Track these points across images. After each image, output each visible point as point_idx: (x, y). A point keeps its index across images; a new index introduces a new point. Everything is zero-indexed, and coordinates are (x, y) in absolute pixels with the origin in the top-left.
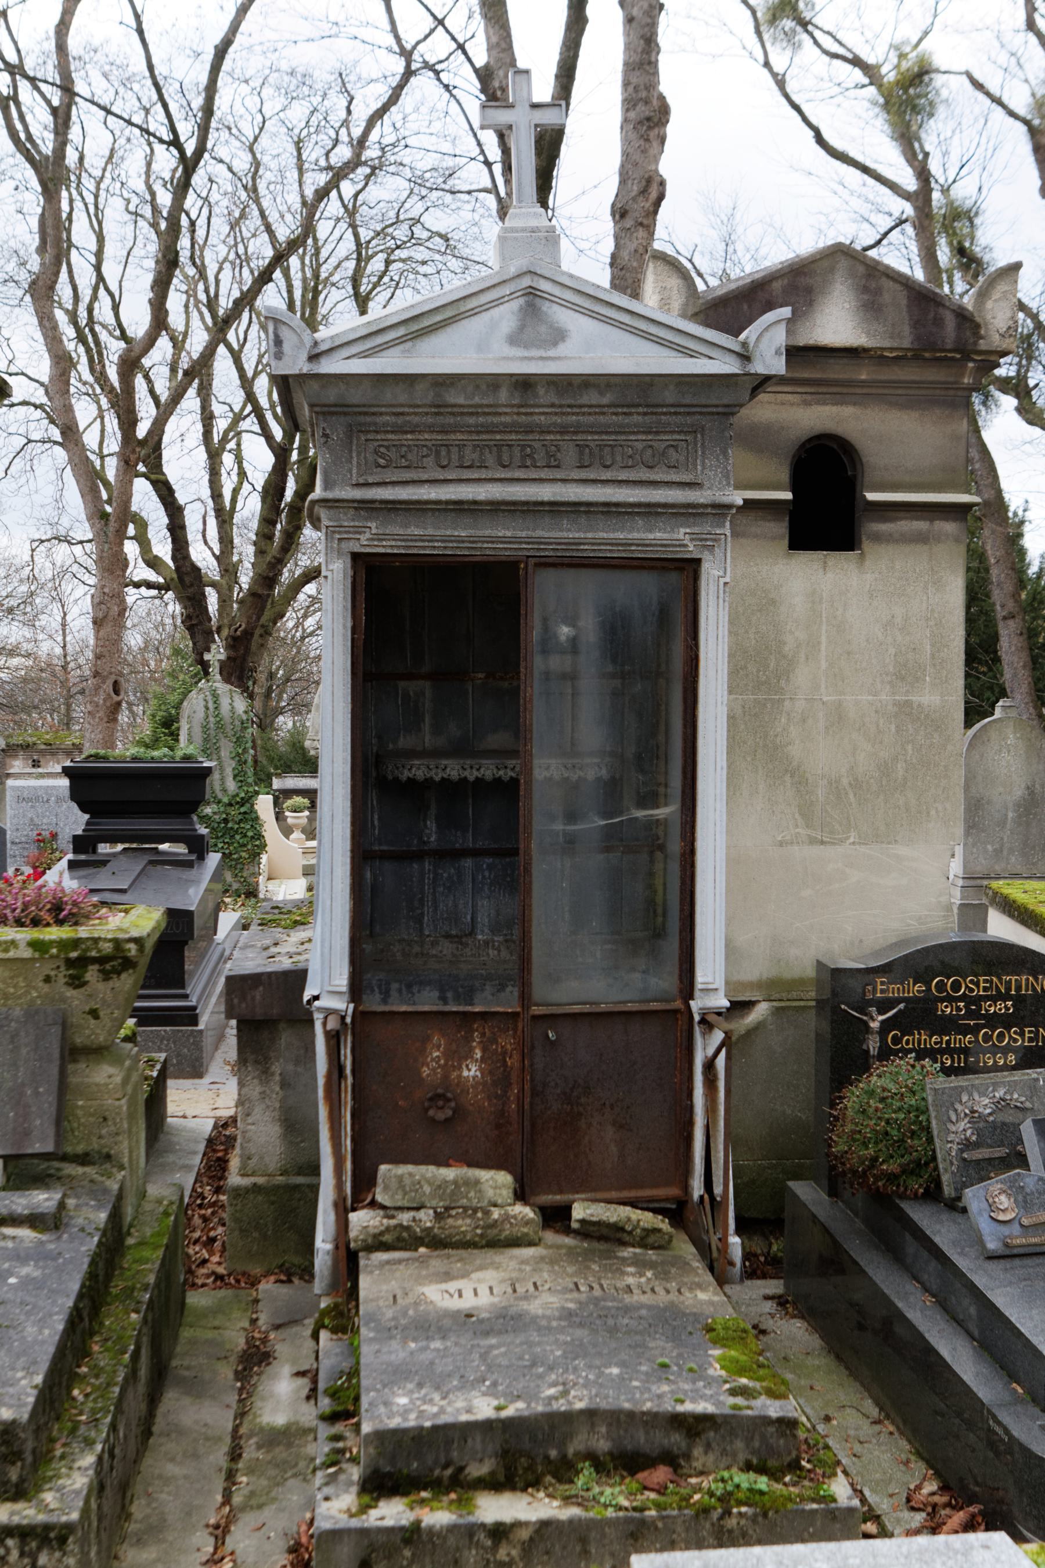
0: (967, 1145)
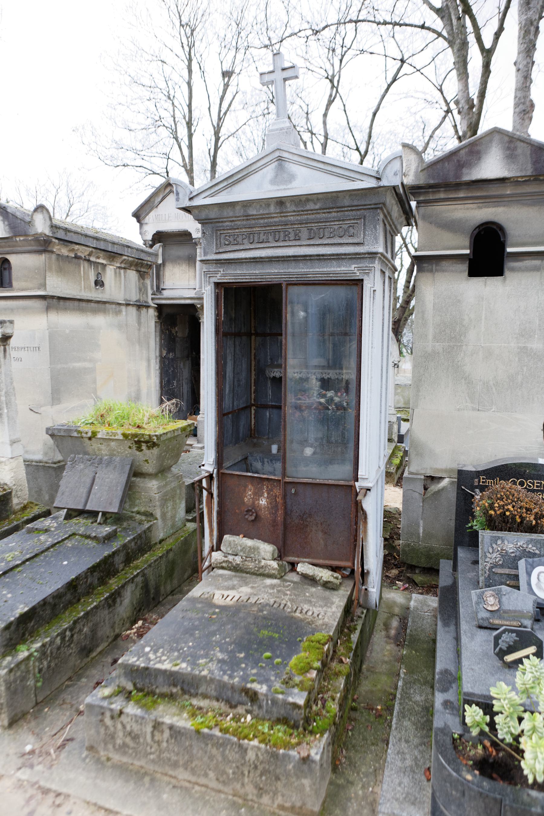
0: (495, 565)
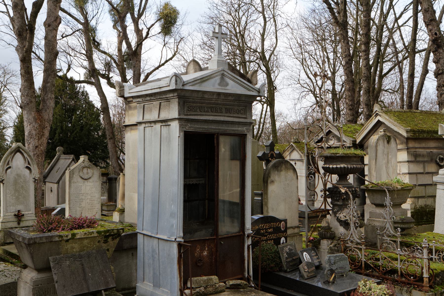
0: (287, 258)
